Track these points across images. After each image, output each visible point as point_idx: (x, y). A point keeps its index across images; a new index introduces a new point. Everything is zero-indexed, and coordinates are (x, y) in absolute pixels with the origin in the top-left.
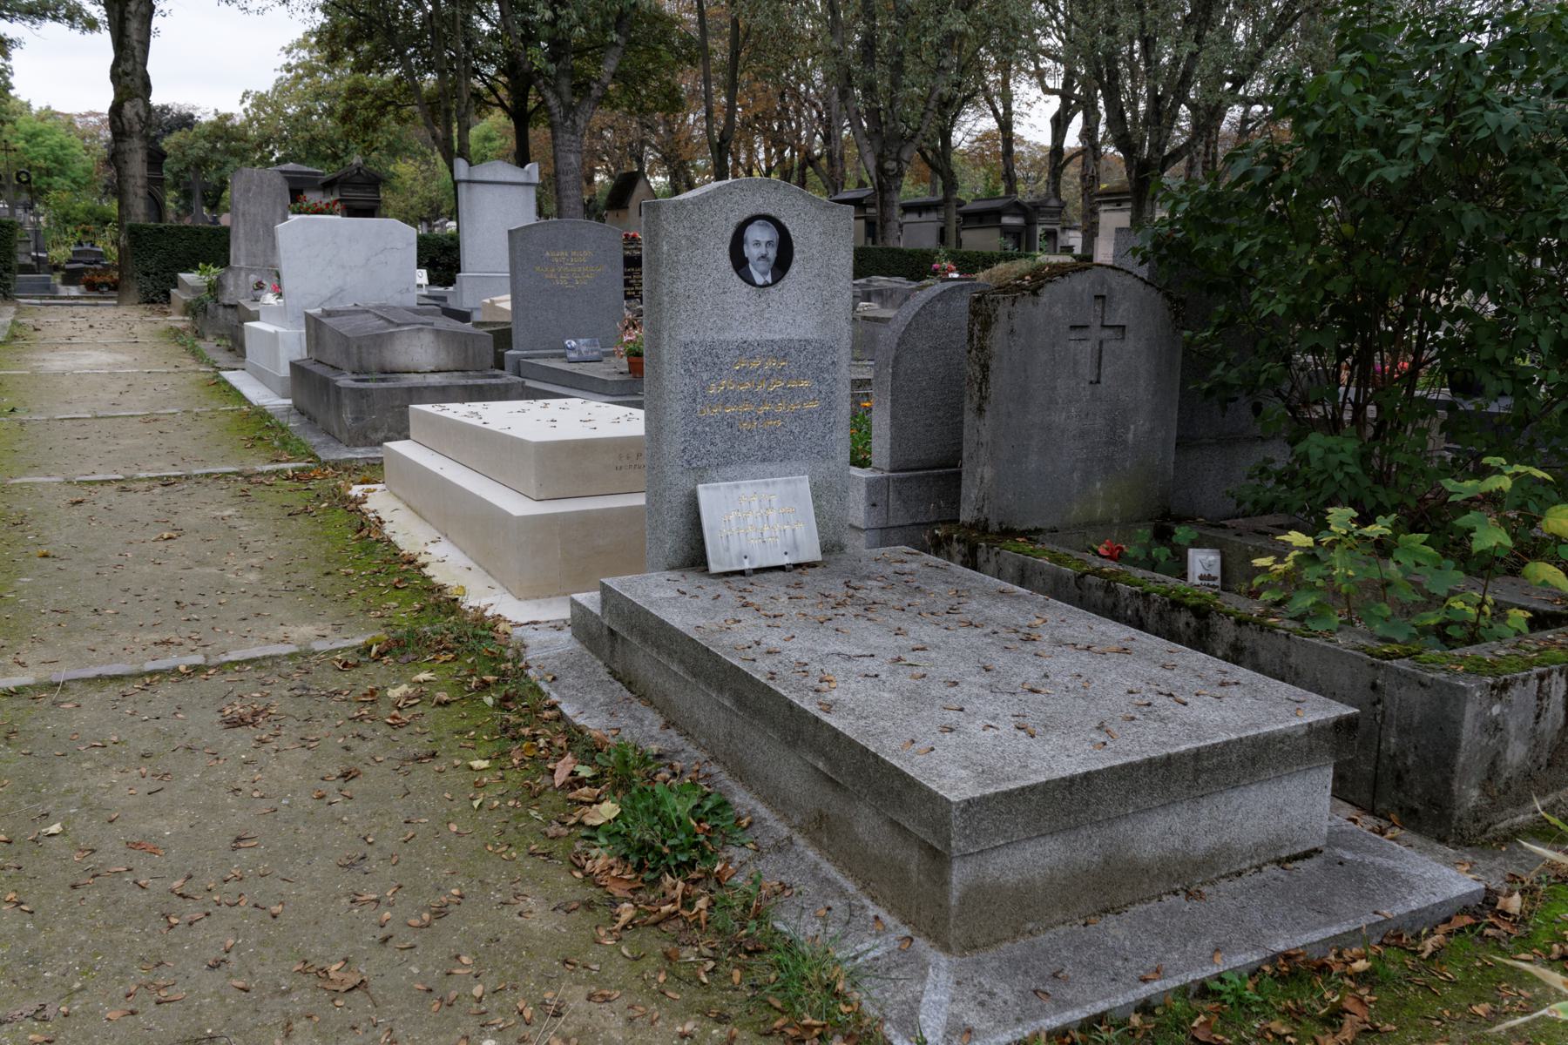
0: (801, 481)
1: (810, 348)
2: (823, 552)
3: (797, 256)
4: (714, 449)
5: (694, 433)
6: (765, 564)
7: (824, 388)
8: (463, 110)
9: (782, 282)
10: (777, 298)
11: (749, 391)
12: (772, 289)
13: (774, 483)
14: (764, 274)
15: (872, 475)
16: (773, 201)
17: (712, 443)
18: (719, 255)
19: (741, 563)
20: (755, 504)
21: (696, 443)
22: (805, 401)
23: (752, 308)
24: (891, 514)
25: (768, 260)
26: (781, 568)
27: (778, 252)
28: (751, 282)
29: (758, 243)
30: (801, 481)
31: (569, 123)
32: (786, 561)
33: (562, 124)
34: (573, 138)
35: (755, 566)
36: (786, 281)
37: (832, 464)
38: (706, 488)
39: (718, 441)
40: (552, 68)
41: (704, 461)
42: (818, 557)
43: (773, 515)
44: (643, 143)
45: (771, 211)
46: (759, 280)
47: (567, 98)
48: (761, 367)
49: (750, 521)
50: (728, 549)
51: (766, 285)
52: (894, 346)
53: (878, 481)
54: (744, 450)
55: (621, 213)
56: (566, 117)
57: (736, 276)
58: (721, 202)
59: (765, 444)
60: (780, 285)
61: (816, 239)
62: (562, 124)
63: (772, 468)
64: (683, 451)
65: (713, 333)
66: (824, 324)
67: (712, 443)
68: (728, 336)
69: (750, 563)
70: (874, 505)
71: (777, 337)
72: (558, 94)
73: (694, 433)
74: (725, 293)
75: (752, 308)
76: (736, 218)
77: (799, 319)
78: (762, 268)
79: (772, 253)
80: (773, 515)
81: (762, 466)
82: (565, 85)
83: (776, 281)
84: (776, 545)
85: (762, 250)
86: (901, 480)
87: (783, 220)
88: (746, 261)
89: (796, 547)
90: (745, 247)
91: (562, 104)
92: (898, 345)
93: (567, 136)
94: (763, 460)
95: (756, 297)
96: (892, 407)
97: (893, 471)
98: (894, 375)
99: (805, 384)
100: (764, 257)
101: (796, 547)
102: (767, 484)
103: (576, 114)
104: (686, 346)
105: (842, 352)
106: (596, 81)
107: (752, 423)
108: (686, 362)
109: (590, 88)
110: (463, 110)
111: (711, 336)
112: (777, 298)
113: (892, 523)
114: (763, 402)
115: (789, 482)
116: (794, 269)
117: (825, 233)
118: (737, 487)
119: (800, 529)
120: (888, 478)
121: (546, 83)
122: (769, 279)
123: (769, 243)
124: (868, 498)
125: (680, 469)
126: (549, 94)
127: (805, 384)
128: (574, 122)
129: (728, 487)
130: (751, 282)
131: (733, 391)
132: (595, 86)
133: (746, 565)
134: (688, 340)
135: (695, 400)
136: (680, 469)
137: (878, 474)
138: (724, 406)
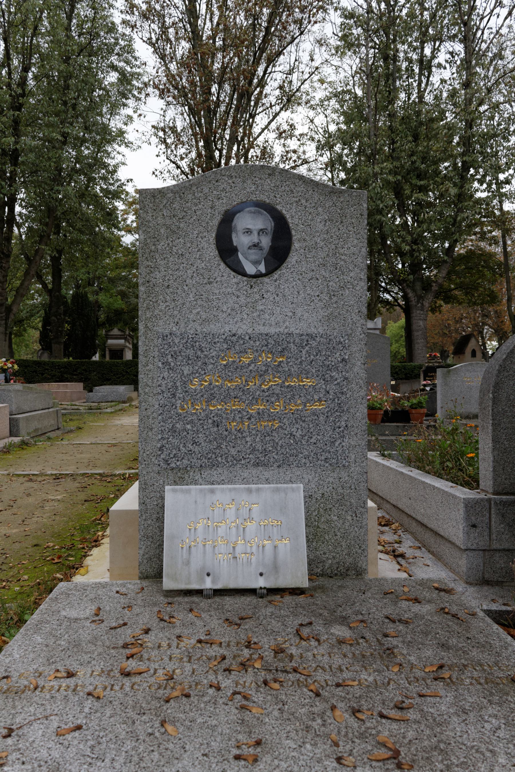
0: (293, 489)
1: (314, 344)
2: (312, 575)
3: (296, 245)
4: (197, 449)
5: (173, 430)
6: (232, 585)
7: (332, 388)
8: (373, 306)
9: (278, 272)
10: (272, 289)
11: (239, 388)
12: (266, 280)
13: (258, 490)
14: (256, 263)
15: (478, 496)
16: (266, 187)
17: (194, 443)
18: (204, 244)
19: (203, 581)
20: (231, 513)
21: (176, 441)
22: (308, 401)
23: (242, 300)
24: (494, 536)
25: (261, 249)
26: (253, 592)
27: (274, 239)
28: (240, 271)
29: (248, 232)
30: (293, 489)
31: (419, 305)
32: (261, 583)
33: (416, 306)
34: (422, 312)
35: (219, 586)
36: (283, 270)
37: (344, 475)
38: (174, 491)
39: (201, 441)
40: (411, 277)
41: (185, 462)
42: (305, 583)
43: (251, 526)
44: (484, 324)
45: (264, 198)
46: (251, 269)
47: (419, 293)
48: (254, 361)
49: (221, 532)
50: (188, 563)
51: (258, 276)
52: (495, 372)
53: (478, 502)
54: (233, 452)
55: (461, 356)
56: (418, 302)
57: (223, 266)
58: (206, 190)
59: (259, 447)
60: (276, 275)
61: (321, 226)
62: (416, 306)
63: (267, 474)
64: (161, 449)
65: (197, 325)
66: (330, 318)
67: (194, 443)
68: (214, 328)
69: (213, 582)
70: (474, 526)
71: (272, 330)
72: (414, 290)
73: (173, 430)
74: (210, 283)
75: (242, 300)
76: (222, 207)
77: (299, 312)
78: (253, 257)
79: (266, 242)
80: (251, 526)
81: (254, 471)
82: (418, 286)
83: (269, 272)
84: (249, 562)
85: (255, 238)
86: (504, 503)
87: (279, 207)
88: (234, 250)
89: (275, 567)
90: (234, 236)
91: (416, 295)
92: (499, 371)
93: (418, 312)
94: (257, 465)
95: (248, 287)
96: (494, 430)
97: (494, 494)
98: (495, 401)
99: (307, 382)
100: (256, 246)
101: (275, 567)
102: (250, 491)
103: (423, 300)
104: (164, 337)
105: (354, 348)
106: (435, 282)
107: (242, 422)
108: (163, 355)
109: (432, 286)
110: (373, 306)
111: (192, 328)
112: (272, 289)
113: (496, 545)
114: (255, 400)
115: (278, 490)
116: (293, 259)
117: (331, 220)
118: (212, 491)
119: (284, 545)
120: (489, 500)
121: (407, 285)
122: (262, 268)
123: (261, 231)
124: (467, 518)
125: (156, 469)
126: (409, 291)
127: (307, 382)
128: (422, 304)
129: (201, 490)
130: (240, 271)
131: (220, 387)
132: (434, 284)
133: (208, 584)
134: (167, 332)
135: (174, 395)
136: (156, 469)
137: (482, 496)
138: (208, 402)
